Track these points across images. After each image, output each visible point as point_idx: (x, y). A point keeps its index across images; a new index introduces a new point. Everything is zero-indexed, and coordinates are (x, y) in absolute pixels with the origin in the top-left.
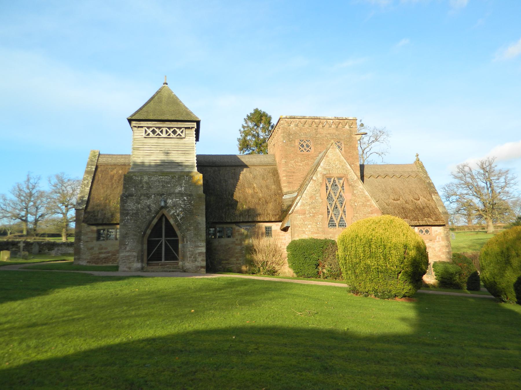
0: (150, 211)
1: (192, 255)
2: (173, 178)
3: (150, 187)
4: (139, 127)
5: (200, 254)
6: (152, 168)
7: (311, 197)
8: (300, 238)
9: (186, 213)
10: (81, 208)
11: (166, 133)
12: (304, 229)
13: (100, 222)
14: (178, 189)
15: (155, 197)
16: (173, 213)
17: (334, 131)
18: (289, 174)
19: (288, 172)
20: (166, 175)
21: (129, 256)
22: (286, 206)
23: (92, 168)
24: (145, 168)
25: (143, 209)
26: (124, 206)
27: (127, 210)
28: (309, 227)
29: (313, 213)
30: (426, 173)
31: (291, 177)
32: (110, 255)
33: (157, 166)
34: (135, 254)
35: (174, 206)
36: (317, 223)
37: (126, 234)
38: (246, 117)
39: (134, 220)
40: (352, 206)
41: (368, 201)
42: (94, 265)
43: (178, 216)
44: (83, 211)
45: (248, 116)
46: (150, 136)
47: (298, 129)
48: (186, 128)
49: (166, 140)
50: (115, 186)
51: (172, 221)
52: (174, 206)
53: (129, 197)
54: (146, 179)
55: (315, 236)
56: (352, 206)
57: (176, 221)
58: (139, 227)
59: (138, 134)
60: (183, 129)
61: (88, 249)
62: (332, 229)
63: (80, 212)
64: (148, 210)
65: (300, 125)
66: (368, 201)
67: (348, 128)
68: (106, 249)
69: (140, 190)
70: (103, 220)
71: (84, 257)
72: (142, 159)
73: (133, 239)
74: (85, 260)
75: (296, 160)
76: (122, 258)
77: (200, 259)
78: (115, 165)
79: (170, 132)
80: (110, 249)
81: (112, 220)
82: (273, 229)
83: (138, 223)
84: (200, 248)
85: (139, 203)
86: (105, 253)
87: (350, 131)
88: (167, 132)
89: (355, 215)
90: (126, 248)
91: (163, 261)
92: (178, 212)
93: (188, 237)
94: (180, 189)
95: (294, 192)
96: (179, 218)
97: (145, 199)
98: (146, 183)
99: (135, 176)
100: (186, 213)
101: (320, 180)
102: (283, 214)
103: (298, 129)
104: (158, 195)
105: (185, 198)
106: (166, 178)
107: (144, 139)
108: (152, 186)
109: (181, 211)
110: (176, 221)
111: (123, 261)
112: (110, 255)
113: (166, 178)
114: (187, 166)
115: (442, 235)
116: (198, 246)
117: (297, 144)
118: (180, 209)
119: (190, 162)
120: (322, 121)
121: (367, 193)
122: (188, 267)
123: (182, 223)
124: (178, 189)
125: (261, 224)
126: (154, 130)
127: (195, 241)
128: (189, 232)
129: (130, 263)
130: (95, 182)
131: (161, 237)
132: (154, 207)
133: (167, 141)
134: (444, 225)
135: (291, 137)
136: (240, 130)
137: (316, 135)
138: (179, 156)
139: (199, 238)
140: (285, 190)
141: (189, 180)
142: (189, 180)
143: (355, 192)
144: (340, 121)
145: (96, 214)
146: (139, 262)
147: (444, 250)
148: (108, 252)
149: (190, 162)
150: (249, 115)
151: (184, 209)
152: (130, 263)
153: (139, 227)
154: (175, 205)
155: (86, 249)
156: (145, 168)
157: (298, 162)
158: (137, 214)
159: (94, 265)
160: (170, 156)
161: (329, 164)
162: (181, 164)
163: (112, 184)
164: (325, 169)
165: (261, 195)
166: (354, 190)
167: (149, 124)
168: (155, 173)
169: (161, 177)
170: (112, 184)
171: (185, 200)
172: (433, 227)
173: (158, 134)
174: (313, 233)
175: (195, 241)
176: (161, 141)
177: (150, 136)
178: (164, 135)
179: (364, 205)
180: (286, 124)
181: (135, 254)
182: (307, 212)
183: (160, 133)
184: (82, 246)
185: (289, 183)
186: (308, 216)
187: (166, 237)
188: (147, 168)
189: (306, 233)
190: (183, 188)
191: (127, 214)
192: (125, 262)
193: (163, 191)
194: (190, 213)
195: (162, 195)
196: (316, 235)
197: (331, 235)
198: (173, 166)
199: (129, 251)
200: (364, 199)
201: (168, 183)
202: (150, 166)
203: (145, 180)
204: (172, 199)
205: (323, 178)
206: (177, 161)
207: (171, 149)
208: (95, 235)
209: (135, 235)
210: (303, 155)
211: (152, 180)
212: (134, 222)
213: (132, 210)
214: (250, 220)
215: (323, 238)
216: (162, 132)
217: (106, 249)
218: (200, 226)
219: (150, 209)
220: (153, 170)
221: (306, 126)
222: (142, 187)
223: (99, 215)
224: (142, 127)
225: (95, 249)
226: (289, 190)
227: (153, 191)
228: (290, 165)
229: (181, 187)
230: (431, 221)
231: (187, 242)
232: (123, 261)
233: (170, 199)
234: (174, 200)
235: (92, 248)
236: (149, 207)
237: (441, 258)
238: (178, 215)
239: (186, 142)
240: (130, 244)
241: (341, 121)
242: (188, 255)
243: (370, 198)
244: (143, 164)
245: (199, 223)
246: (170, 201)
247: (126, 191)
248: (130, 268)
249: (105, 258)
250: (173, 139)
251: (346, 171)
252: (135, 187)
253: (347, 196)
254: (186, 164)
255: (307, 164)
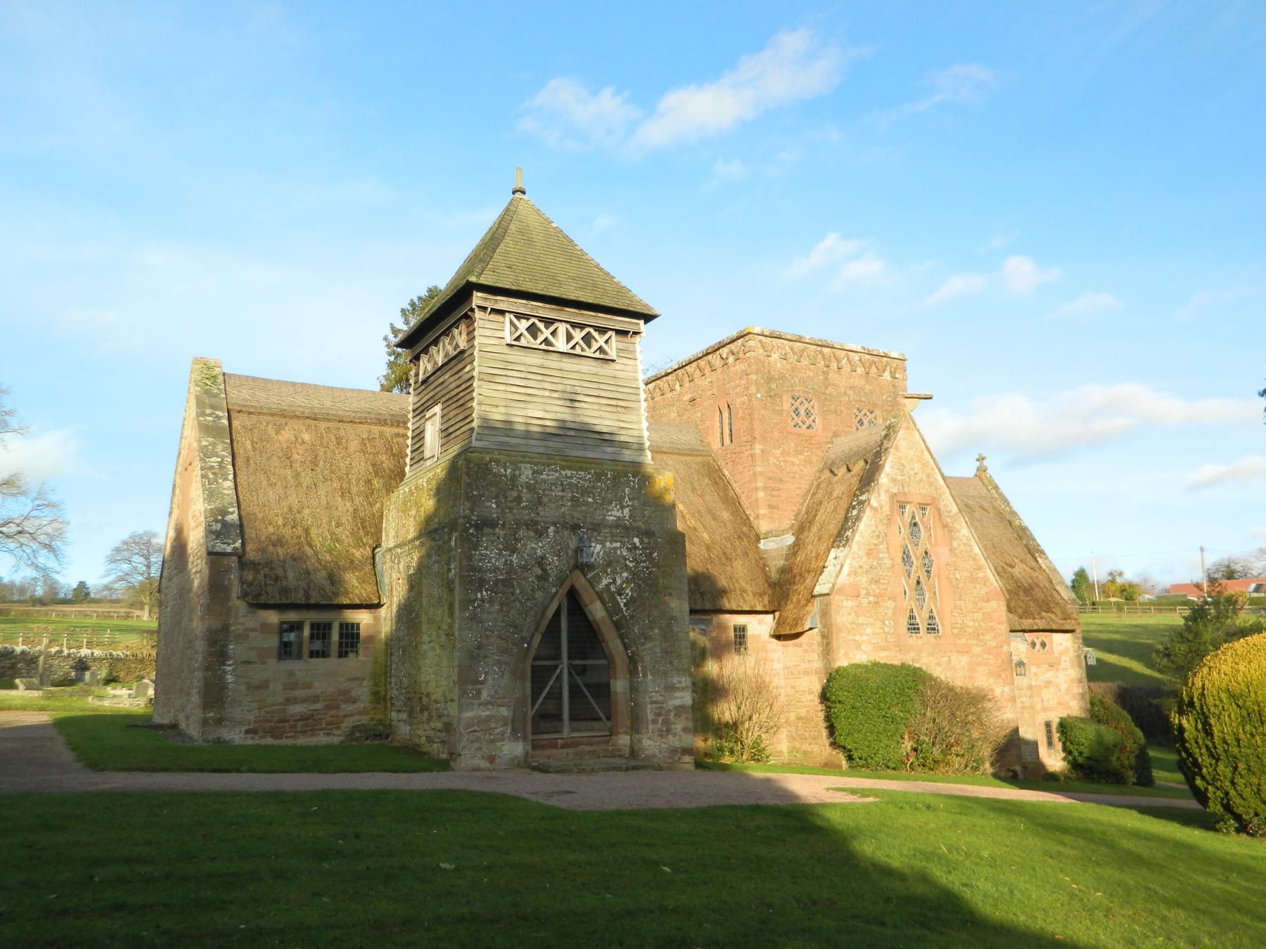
0: (543, 577)
1: (659, 714)
2: (598, 477)
3: (540, 502)
4: (494, 311)
5: (680, 710)
6: (533, 442)
7: (869, 553)
8: (853, 662)
9: (639, 586)
10: (229, 549)
11: (568, 341)
12: (858, 638)
13: (300, 598)
14: (615, 513)
15: (556, 532)
16: (608, 586)
17: (862, 382)
18: (771, 484)
19: (770, 478)
20: (581, 469)
21: (489, 718)
22: (773, 570)
23: (219, 418)
24: (515, 441)
25: (525, 568)
26: (470, 558)
27: (480, 570)
28: (868, 630)
29: (875, 596)
30: (1006, 501)
31: (775, 493)
32: (320, 706)
33: (547, 436)
34: (504, 712)
35: (609, 564)
36: (883, 622)
37: (479, 648)
38: (407, 306)
39: (502, 604)
40: (950, 581)
41: (980, 568)
42: (269, 741)
43: (620, 595)
44: (235, 558)
45: (413, 304)
46: (523, 342)
47: (788, 367)
48: (619, 332)
49: (566, 359)
50: (306, 479)
51: (597, 611)
52: (609, 564)
53: (486, 530)
54: (526, 474)
55: (885, 657)
56: (950, 581)
57: (613, 610)
58: (515, 627)
59: (488, 333)
60: (610, 333)
61: (250, 687)
62: (913, 640)
63: (225, 561)
64: (539, 572)
65: (793, 358)
66: (980, 568)
67: (889, 379)
68: (308, 686)
69: (511, 509)
70: (308, 598)
71: (237, 713)
72: (503, 410)
73: (498, 663)
74: (241, 723)
75: (786, 447)
76: (468, 726)
77: (678, 727)
78: (283, 415)
79: (578, 335)
80: (318, 688)
81: (336, 594)
82: (750, 632)
83: (513, 612)
84: (678, 694)
85: (513, 550)
86: (304, 700)
87: (894, 386)
88: (569, 337)
89: (958, 603)
90: (479, 692)
91: (566, 732)
92: (619, 582)
93: (647, 658)
94: (619, 514)
95: (783, 532)
96: (621, 601)
97: (529, 538)
98: (530, 488)
99: (497, 462)
100: (639, 586)
101: (886, 509)
102: (784, 591)
103: (788, 367)
104: (564, 526)
105: (636, 540)
106: (580, 478)
107: (507, 350)
108: (545, 500)
109: (627, 581)
110: (613, 610)
111: (472, 737)
112: (320, 706)
113: (580, 478)
114: (625, 445)
115: (1071, 654)
116: (671, 688)
117: (786, 406)
118: (625, 575)
119: (630, 432)
120: (838, 353)
121: (976, 550)
122: (648, 752)
123: (632, 617)
124: (614, 514)
125: (727, 616)
126: (533, 324)
127: (665, 673)
128: (648, 645)
129: (492, 741)
130: (239, 461)
131: (557, 656)
132: (554, 563)
133: (568, 364)
134: (1072, 631)
135: (774, 386)
136: (386, 339)
137: (826, 388)
138: (603, 415)
139: (676, 662)
140: (763, 526)
141: (640, 489)
142: (640, 489)
143: (955, 544)
144: (876, 361)
145: (280, 572)
146: (517, 739)
147: (1075, 691)
148: (315, 699)
149: (630, 432)
150: (416, 300)
151: (635, 576)
152: (492, 741)
153: (515, 627)
154: (611, 562)
155: (243, 688)
156: (515, 441)
157: (789, 454)
158: (507, 582)
159: (269, 741)
160: (579, 412)
161: (902, 467)
162: (607, 437)
163: (297, 475)
164: (894, 480)
165: (705, 535)
166: (952, 539)
167: (520, 305)
168: (548, 460)
169: (569, 473)
170: (297, 475)
171: (636, 548)
172: (1055, 635)
173: (546, 341)
174: (879, 648)
175: (665, 673)
176: (553, 362)
177: (523, 342)
178: (561, 344)
179: (974, 580)
180: (761, 351)
181: (504, 712)
182: (863, 592)
183: (550, 337)
184: (230, 678)
185: (771, 507)
186: (865, 602)
187: (570, 658)
188: (521, 441)
189: (863, 647)
190: (626, 511)
191: (481, 583)
192: (478, 740)
193: (576, 515)
194: (650, 586)
195: (575, 528)
196: (883, 654)
197: (912, 654)
198: (588, 442)
199: (489, 703)
200: (972, 563)
201: (586, 492)
202: (527, 435)
203: (523, 479)
204: (603, 543)
205: (892, 504)
206: (598, 429)
207: (579, 390)
208: (273, 642)
209: (504, 651)
210: (799, 435)
211: (544, 481)
212: (501, 610)
213: (495, 570)
214: (708, 606)
215: (897, 662)
216: (554, 333)
217: (309, 686)
218: (676, 629)
219: (544, 570)
220: (537, 446)
221: (805, 362)
222: (518, 499)
223: (291, 576)
224: (502, 312)
225: (272, 686)
226: (772, 527)
227: (547, 513)
228: (772, 460)
229: (622, 508)
230: (1058, 623)
231: (645, 676)
232: (472, 737)
233: (597, 541)
234: (608, 544)
235: (263, 685)
236: (541, 562)
237: (1069, 708)
238: (620, 592)
239: (620, 374)
240: (490, 681)
241: (876, 359)
242: (649, 713)
243: (983, 561)
244: (507, 428)
245: (674, 618)
246: (599, 547)
247: (472, 511)
248: (491, 759)
249: (304, 718)
250: (583, 361)
251: (936, 489)
252: (497, 497)
253: (941, 555)
254: (622, 439)
255: (808, 462)
